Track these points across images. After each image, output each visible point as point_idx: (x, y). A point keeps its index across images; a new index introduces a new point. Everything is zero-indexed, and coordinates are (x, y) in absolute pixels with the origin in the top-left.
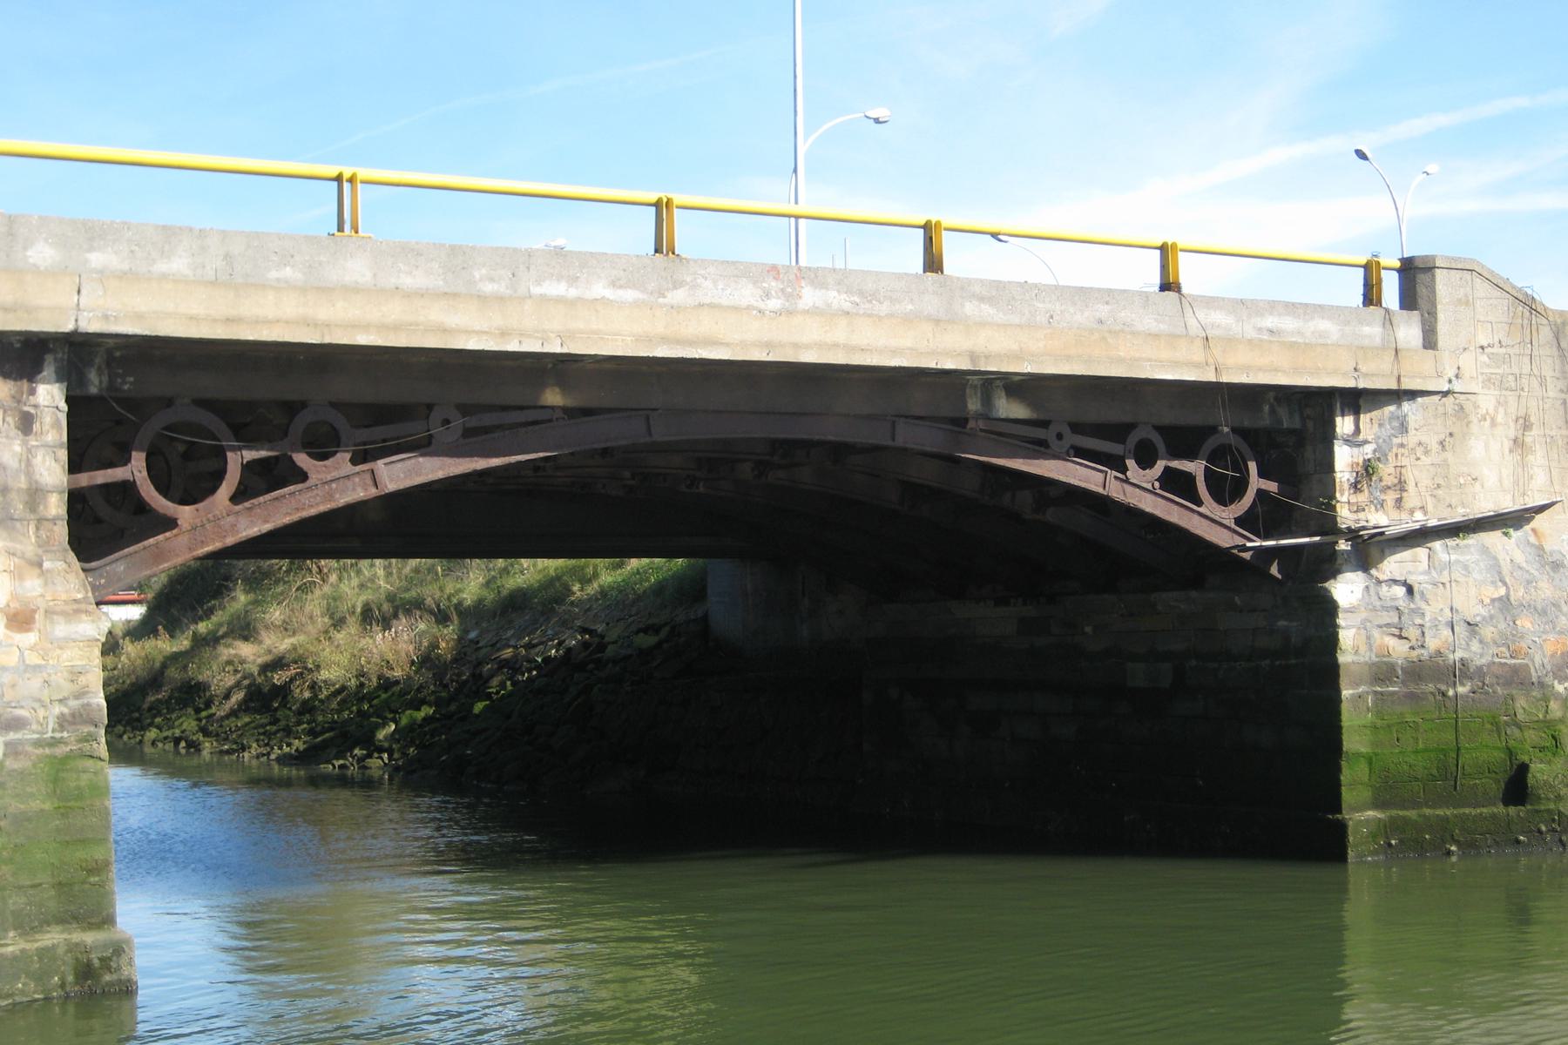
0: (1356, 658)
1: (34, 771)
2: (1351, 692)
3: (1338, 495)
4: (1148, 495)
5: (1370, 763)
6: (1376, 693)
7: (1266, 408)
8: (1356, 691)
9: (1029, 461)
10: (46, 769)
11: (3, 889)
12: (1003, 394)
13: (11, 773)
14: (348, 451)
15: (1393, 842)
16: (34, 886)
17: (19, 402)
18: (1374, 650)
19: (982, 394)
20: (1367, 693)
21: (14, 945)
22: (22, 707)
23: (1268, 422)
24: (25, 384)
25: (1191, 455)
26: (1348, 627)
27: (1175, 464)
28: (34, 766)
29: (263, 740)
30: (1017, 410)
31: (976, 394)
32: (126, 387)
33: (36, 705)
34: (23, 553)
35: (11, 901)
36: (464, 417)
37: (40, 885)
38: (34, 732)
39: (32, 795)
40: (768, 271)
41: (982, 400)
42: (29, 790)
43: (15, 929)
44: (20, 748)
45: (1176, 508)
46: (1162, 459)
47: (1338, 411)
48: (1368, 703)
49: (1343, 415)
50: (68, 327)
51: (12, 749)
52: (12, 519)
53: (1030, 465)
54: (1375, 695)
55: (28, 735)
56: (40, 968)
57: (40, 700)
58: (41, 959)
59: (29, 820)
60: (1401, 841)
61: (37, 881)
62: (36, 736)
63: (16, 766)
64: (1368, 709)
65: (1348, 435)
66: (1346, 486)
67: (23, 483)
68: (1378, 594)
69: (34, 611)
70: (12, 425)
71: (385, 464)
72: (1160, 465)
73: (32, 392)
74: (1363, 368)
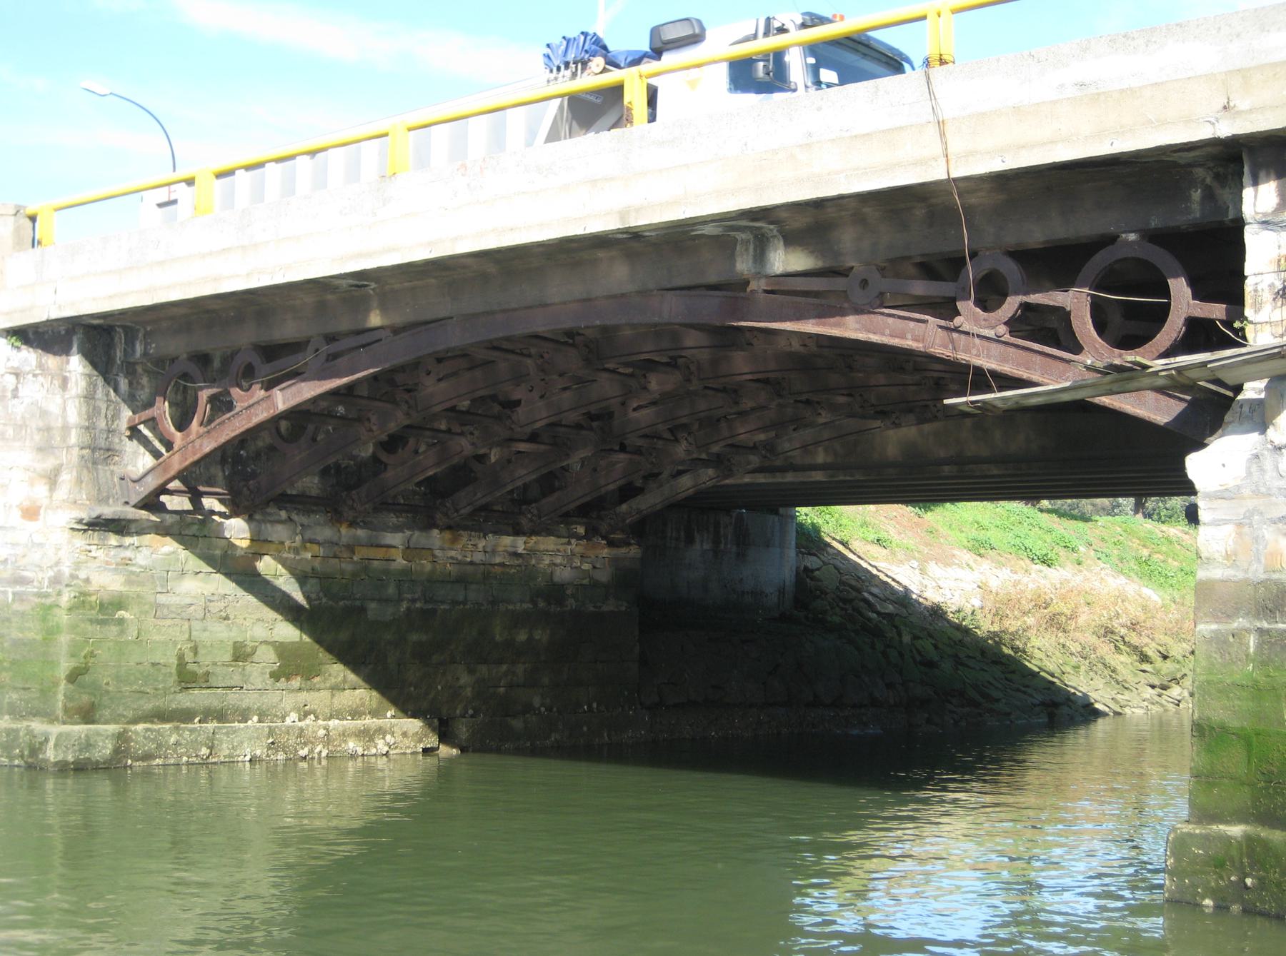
0: (1229, 573)
1: (31, 613)
2: (1214, 627)
3: (1248, 312)
4: (993, 345)
5: (1249, 745)
6: (1261, 631)
7: (1197, 195)
8: (1222, 627)
9: (823, 320)
10: (41, 613)
11: (3, 687)
12: (782, 243)
13: (16, 613)
14: (257, 383)
15: (1249, 881)
16: (24, 689)
17: (62, 370)
18: (1263, 561)
19: (755, 250)
20: (1248, 631)
21: (2, 723)
22: (27, 570)
23: (1198, 215)
24: (64, 357)
25: (1064, 283)
26: (1216, 523)
27: (1036, 298)
28: (33, 609)
29: (1057, 658)
30: (784, 260)
31: (747, 250)
32: (151, 351)
33: (37, 569)
34: (35, 469)
35: (7, 696)
36: (328, 344)
37: (29, 688)
38: (34, 587)
39: (29, 629)
40: (458, 170)
41: (755, 257)
42: (27, 625)
43: (10, 715)
44: (25, 597)
45: (1038, 358)
46: (1016, 293)
47: (1247, 178)
48: (1248, 648)
49: (1255, 183)
50: (44, 318)
51: (18, 597)
52: (53, 447)
53: (824, 325)
54: (1261, 635)
55: (30, 589)
56: (7, 741)
57: (39, 566)
58: (8, 735)
59: (25, 644)
60: (1261, 880)
61: (27, 686)
62: (35, 590)
63: (19, 609)
64: (1247, 656)
65: (1265, 214)
66: (1267, 296)
67: (59, 424)
68: (1278, 468)
69: (40, 507)
70: (57, 385)
71: (280, 390)
72: (1011, 305)
73: (68, 362)
74: (1241, 103)
